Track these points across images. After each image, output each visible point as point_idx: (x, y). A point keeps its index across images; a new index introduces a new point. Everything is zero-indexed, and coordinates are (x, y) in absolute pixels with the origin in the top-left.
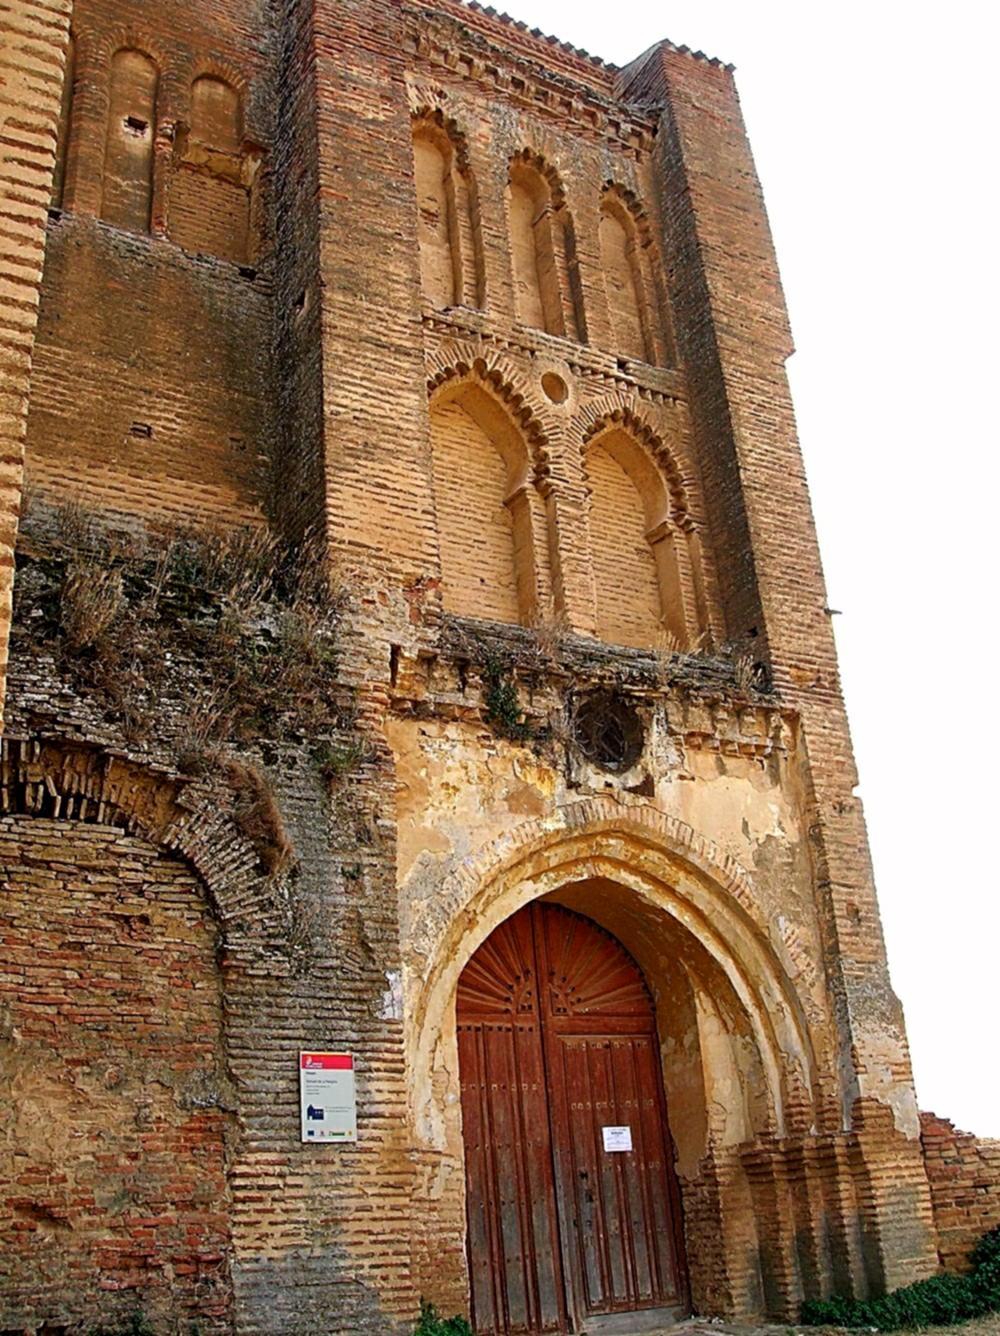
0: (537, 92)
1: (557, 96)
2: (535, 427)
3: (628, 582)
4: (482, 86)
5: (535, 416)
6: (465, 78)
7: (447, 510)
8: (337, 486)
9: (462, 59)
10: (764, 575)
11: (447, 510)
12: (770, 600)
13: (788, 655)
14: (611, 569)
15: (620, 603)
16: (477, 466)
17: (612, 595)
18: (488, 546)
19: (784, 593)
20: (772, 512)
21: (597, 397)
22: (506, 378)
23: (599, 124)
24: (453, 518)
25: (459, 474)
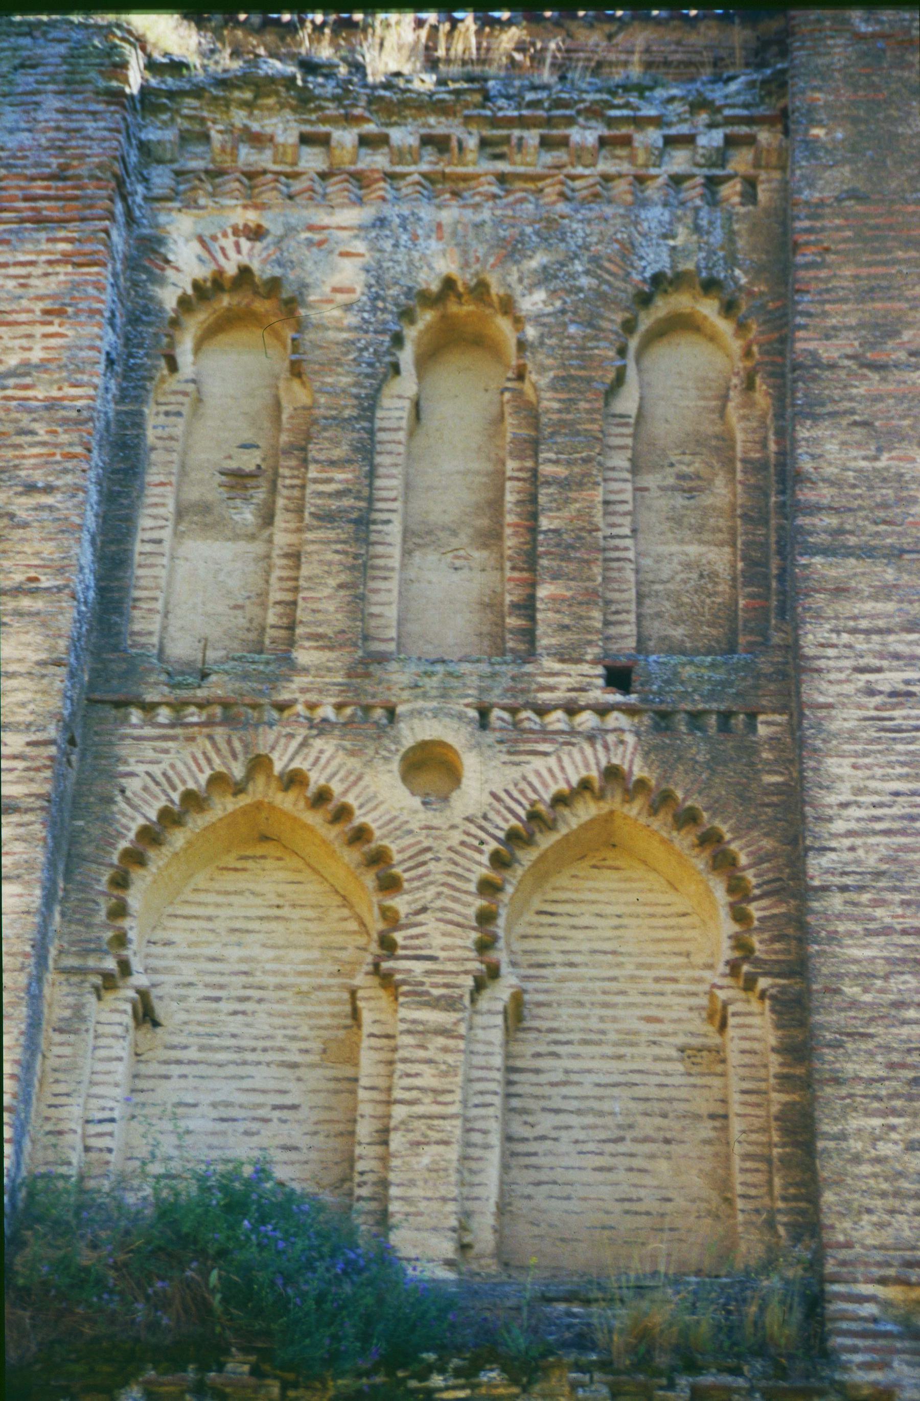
0: (484, 143)
1: (532, 136)
2: (378, 859)
3: (647, 1126)
4: (360, 179)
5: (380, 838)
6: (323, 176)
7: (222, 1056)
8: (541, 997)
9: (305, 139)
10: (837, 1081)
11: (222, 1056)
12: (843, 1136)
13: (878, 1256)
14: (606, 1106)
15: (621, 1175)
16: (303, 954)
17: (600, 1161)
18: (300, 1115)
19: (884, 1114)
20: (887, 931)
21: (538, 763)
22: (316, 779)
23: (641, 158)
24: (231, 1070)
25: (259, 978)
